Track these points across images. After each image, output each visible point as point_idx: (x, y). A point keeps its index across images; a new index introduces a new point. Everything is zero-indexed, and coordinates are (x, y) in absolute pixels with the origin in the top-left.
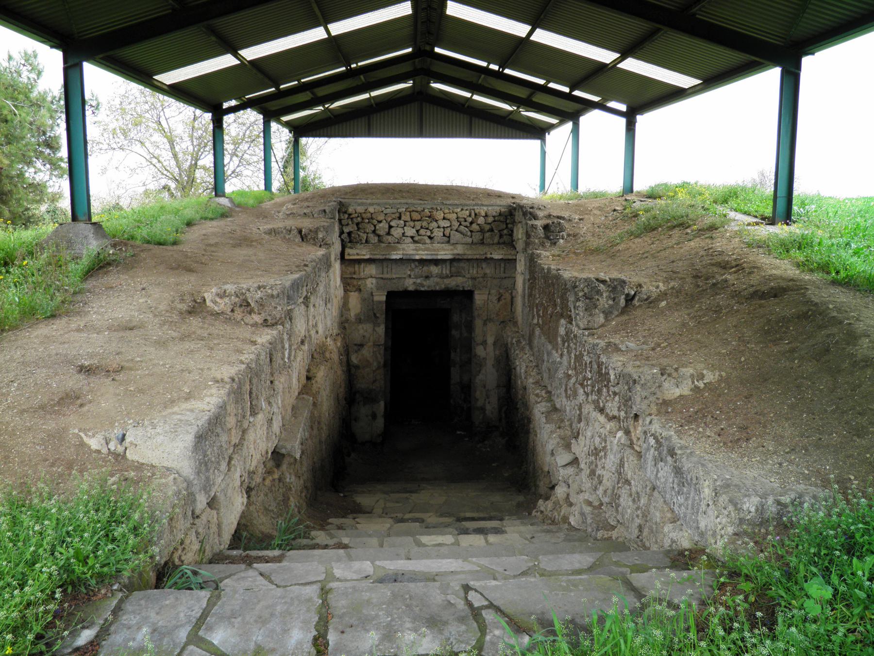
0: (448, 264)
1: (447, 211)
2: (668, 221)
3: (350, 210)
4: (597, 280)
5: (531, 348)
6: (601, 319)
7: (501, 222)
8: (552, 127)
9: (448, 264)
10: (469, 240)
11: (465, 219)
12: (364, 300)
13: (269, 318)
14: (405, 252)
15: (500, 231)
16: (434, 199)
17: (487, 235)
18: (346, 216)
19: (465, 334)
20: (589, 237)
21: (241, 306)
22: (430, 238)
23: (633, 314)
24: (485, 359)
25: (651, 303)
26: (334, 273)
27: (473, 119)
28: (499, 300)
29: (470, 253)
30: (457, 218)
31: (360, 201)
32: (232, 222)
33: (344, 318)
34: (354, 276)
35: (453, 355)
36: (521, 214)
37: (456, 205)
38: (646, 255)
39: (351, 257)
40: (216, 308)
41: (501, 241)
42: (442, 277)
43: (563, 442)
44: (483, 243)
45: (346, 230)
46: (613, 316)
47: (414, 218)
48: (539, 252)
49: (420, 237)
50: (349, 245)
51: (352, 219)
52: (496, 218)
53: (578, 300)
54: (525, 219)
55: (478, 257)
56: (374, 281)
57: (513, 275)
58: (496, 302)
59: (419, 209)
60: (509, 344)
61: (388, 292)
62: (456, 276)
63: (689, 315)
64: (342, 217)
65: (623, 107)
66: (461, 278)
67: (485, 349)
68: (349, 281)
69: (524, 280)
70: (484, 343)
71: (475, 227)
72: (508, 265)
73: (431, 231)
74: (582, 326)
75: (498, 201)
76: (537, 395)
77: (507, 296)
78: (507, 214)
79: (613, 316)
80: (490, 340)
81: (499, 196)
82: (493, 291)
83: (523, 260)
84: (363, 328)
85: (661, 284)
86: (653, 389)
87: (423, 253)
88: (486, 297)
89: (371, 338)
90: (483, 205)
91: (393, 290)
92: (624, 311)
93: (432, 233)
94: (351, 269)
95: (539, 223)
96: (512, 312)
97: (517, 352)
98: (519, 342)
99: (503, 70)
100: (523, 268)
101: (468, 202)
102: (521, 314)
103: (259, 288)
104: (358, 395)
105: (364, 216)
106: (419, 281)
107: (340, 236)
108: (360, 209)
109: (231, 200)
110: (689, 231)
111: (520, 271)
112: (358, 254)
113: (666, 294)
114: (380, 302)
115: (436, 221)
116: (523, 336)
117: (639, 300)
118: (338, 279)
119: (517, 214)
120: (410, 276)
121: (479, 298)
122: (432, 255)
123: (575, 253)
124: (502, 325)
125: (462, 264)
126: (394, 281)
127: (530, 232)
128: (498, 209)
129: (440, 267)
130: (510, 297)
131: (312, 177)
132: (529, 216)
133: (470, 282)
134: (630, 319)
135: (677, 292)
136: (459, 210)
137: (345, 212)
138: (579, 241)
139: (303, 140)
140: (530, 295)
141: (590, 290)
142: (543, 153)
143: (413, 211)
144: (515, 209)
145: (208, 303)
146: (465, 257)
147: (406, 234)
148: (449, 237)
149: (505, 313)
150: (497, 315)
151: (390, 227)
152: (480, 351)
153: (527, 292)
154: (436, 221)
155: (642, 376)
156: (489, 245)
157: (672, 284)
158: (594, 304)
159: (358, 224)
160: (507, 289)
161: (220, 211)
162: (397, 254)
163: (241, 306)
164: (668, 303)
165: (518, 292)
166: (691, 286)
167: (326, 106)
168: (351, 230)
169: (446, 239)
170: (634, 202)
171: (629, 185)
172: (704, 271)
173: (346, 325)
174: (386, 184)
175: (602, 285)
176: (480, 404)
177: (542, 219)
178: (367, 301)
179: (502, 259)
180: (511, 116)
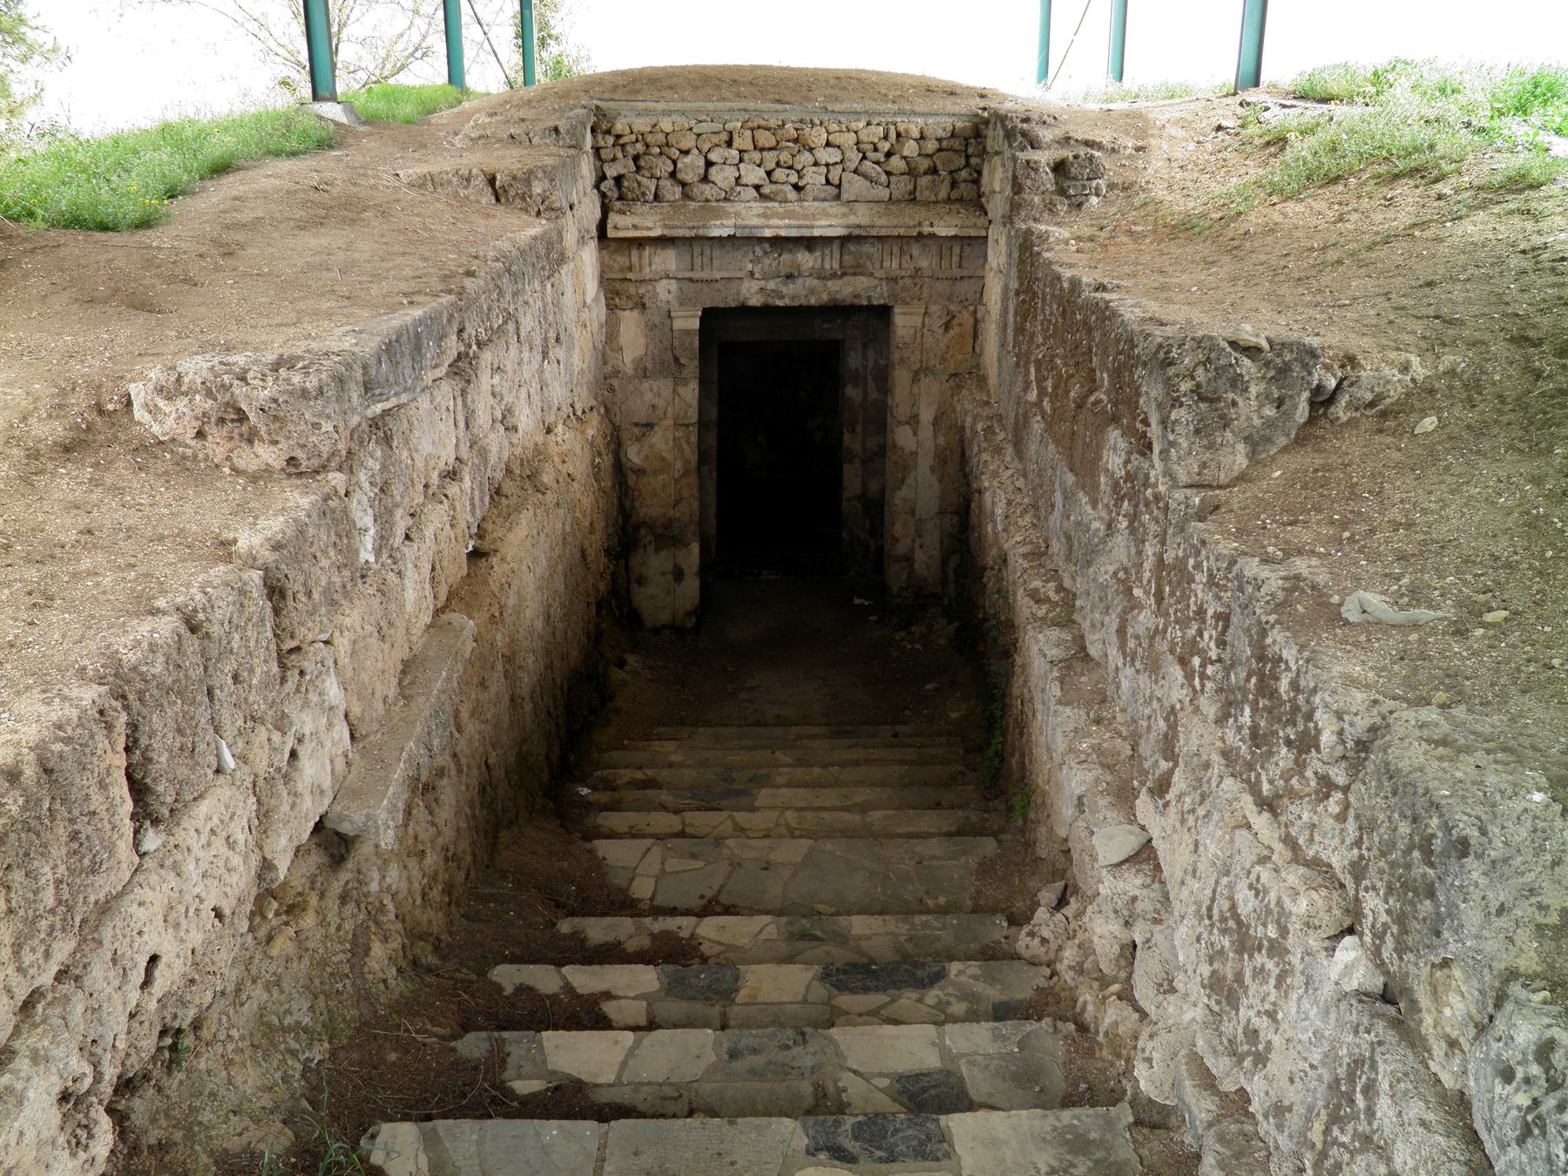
0: (836, 247)
1: (834, 127)
2: (1371, 159)
3: (619, 127)
4: (1233, 344)
5: (1020, 454)
7: (955, 151)
9: (836, 247)
10: (884, 193)
11: (875, 144)
12: (652, 327)
14: (739, 222)
15: (951, 172)
16: (807, 99)
17: (924, 181)
18: (610, 140)
19: (874, 395)
20: (1159, 192)
21: (221, 421)
22: (796, 187)
23: (1336, 450)
24: (914, 454)
25: (1384, 415)
26: (577, 274)
28: (947, 327)
29: (885, 223)
30: (858, 143)
31: (641, 105)
32: (339, 159)
33: (608, 369)
34: (629, 276)
35: (847, 438)
36: (1002, 133)
37: (856, 113)
38: (1332, 255)
39: (621, 234)
40: (156, 429)
42: (822, 276)
43: (1109, 778)
44: (915, 199)
45: (611, 172)
47: (760, 144)
49: (774, 187)
50: (618, 205)
51: (623, 146)
52: (945, 144)
53: (1177, 403)
54: (1010, 146)
55: (902, 232)
56: (673, 285)
57: (979, 273)
58: (941, 331)
59: (773, 123)
60: (968, 431)
61: (705, 311)
62: (855, 274)
63: (1537, 481)
64: (602, 144)
66: (863, 279)
67: (915, 434)
68: (618, 285)
69: (1006, 289)
70: (914, 420)
71: (896, 163)
73: (798, 172)
74: (1183, 477)
75: (950, 105)
76: (1038, 599)
77: (966, 318)
79: (1274, 450)
80: (927, 415)
82: (934, 308)
83: (1003, 241)
84: (651, 390)
85: (1415, 360)
86: (1530, 877)
87: (780, 223)
88: (918, 320)
90: (914, 113)
91: (714, 305)
93: (800, 177)
94: (622, 260)
95: (1044, 158)
96: (976, 353)
97: (985, 456)
98: (989, 430)
100: (1003, 260)
101: (882, 107)
103: (276, 366)
104: (643, 531)
105: (649, 138)
106: (771, 285)
107: (597, 186)
108: (642, 125)
109: (349, 107)
110: (1447, 191)
111: (994, 265)
112: (635, 227)
113: (1431, 391)
114: (687, 332)
115: (811, 150)
116: (1000, 418)
117: (1353, 406)
118: (592, 287)
120: (752, 274)
121: (904, 322)
122: (800, 227)
123: (1130, 233)
125: (867, 248)
126: (718, 286)
127: (1021, 180)
128: (948, 122)
129: (818, 254)
130: (972, 320)
131: (574, 55)
132: (1020, 139)
134: (1327, 468)
135: (1466, 386)
136: (861, 124)
137: (608, 132)
138: (1137, 202)
140: (1020, 330)
143: (759, 127)
144: (986, 122)
145: (139, 413)
147: (744, 181)
148: (839, 186)
149: (960, 357)
151: (709, 164)
152: (904, 437)
154: (811, 150)
155: (1494, 830)
156: (927, 203)
157: (1448, 360)
160: (964, 303)
161: (316, 134)
163: (221, 421)
164: (1442, 425)
165: (988, 312)
166: (1511, 371)
168: (623, 171)
169: (832, 191)
170: (1267, 109)
171: (1249, 67)
172: (1545, 321)
173: (615, 382)
174: (704, 67)
175: (1247, 362)
176: (901, 548)
177: (1049, 147)
178: (660, 328)
179: (955, 237)
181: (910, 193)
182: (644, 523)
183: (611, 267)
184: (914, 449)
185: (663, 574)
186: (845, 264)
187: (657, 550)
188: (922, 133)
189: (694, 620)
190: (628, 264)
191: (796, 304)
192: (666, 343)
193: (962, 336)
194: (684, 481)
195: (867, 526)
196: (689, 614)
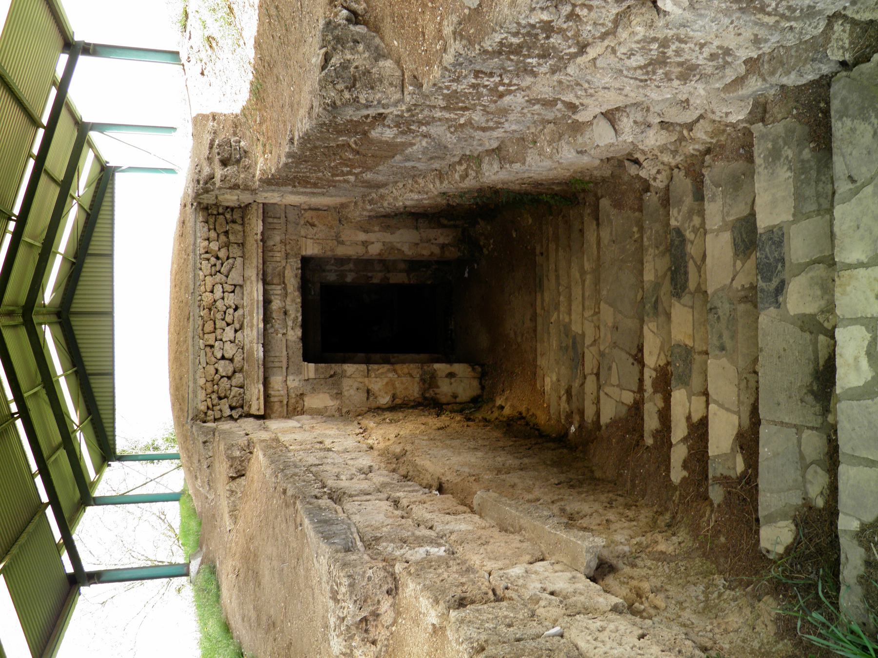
0: (269, 287)
1: (202, 288)
4: (323, 68)
5: (384, 185)
6: (387, 65)
7: (215, 221)
8: (97, 158)
9: (269, 287)
10: (239, 261)
11: (212, 266)
13: (385, 588)
14: (255, 341)
15: (227, 223)
17: (232, 238)
18: (210, 412)
19: (351, 266)
21: (366, 631)
22: (236, 309)
23: (382, 10)
27: (90, 252)
28: (313, 225)
29: (255, 260)
30: (211, 275)
33: (337, 414)
34: (285, 402)
36: (206, 195)
38: (273, 12)
39: (262, 407)
41: (239, 221)
43: (567, 136)
45: (227, 412)
46: (382, 45)
47: (212, 329)
48: (258, 172)
49: (236, 322)
50: (246, 408)
52: (211, 227)
53: (356, 100)
54: (213, 190)
55: (260, 250)
56: (290, 378)
58: (315, 229)
59: (200, 322)
60: (371, 214)
61: (304, 360)
62: (284, 277)
64: (212, 417)
65: (64, 58)
66: (286, 272)
67: (373, 243)
68: (290, 409)
69: (292, 193)
70: (365, 244)
71: (222, 254)
72: (269, 215)
73: (227, 308)
74: (398, 96)
75: (190, 224)
77: (308, 215)
78: (205, 214)
79: (382, 45)
80: (362, 236)
81: (184, 223)
82: (303, 233)
83: (266, 195)
84: (348, 390)
87: (255, 319)
88: (310, 242)
89: (359, 380)
90: (195, 244)
92: (377, 30)
93: (230, 307)
94: (277, 407)
95: (219, 172)
96: (328, 209)
98: (371, 202)
99: (15, 216)
100: (276, 194)
101: (191, 262)
102: (334, 198)
104: (427, 395)
105: (209, 391)
106: (290, 323)
107: (236, 420)
108: (201, 395)
109: (191, 557)
111: (279, 199)
112: (258, 399)
114: (316, 370)
115: (215, 301)
116: (364, 196)
119: (205, 202)
121: (311, 249)
122: (258, 307)
124: (344, 222)
125: (269, 270)
128: (199, 225)
129: (273, 298)
132: (209, 185)
133: (292, 260)
134: (392, 15)
136: (201, 273)
137: (206, 413)
139: (118, 451)
140: (315, 185)
141: (340, 80)
142: (131, 169)
143: (203, 330)
144: (199, 203)
146: (261, 266)
147: (232, 339)
148: (235, 286)
150: (331, 227)
152: (375, 250)
153: (308, 190)
154: (215, 301)
156: (244, 237)
158: (364, 74)
159: (220, 398)
160: (300, 216)
162: (257, 350)
167: (75, 427)
169: (238, 289)
173: (344, 410)
175: (333, 61)
176: (437, 251)
177: (213, 169)
178: (314, 385)
179: (263, 221)
180: (87, 207)
181: (239, 246)
182: (422, 394)
183: (281, 412)
184: (381, 244)
185: (451, 384)
186: (278, 282)
187: (438, 387)
188: (206, 240)
189: (477, 367)
190: (278, 403)
191: (300, 309)
192: (322, 382)
193: (318, 216)
194: (399, 372)
195: (424, 270)
196: (474, 369)
